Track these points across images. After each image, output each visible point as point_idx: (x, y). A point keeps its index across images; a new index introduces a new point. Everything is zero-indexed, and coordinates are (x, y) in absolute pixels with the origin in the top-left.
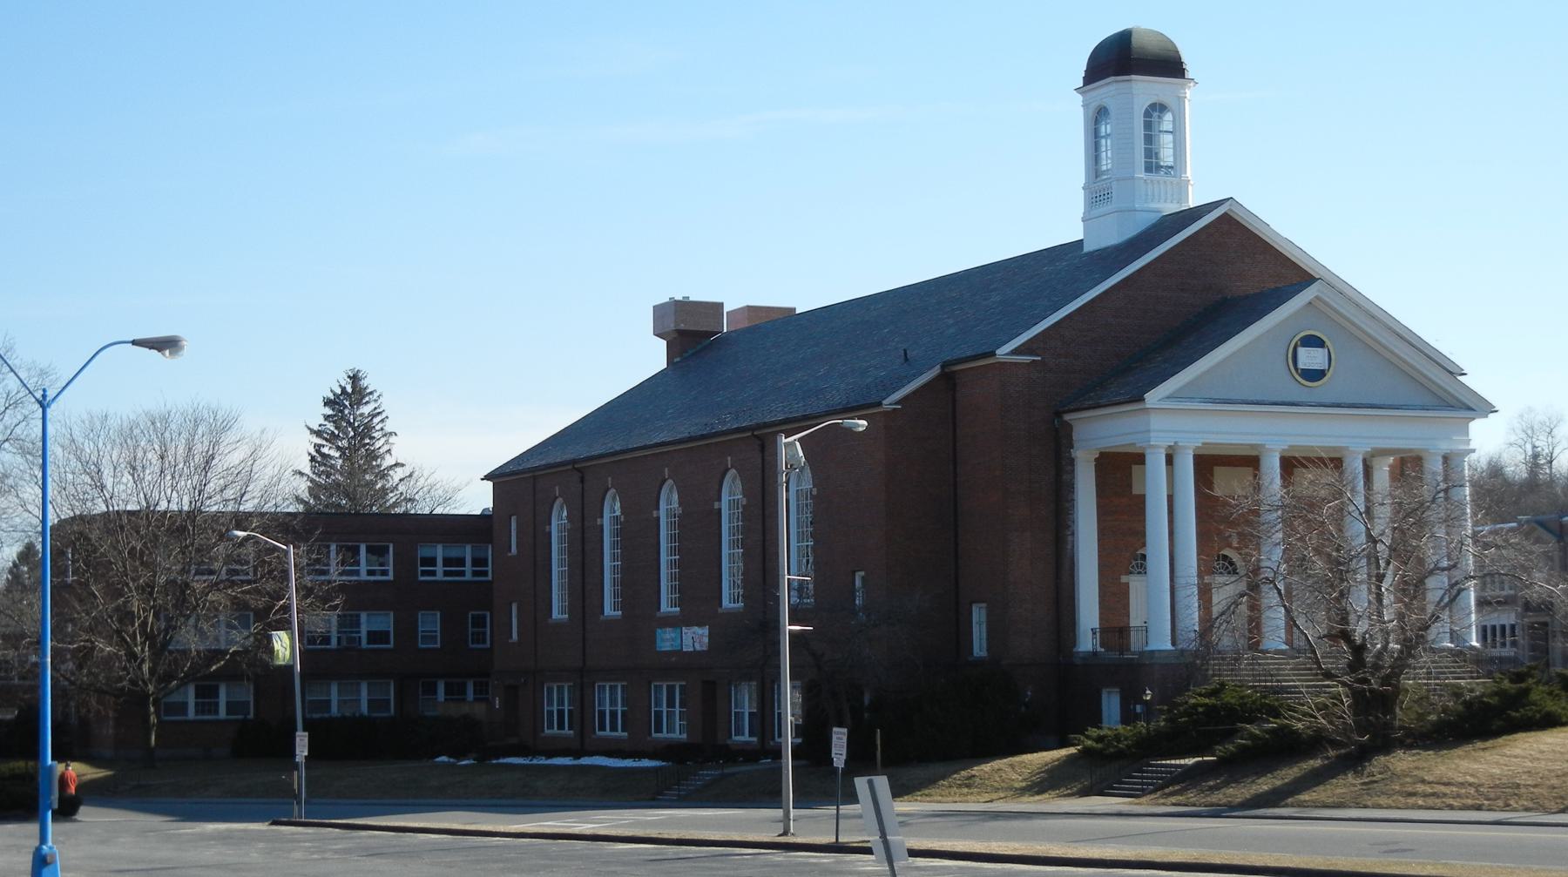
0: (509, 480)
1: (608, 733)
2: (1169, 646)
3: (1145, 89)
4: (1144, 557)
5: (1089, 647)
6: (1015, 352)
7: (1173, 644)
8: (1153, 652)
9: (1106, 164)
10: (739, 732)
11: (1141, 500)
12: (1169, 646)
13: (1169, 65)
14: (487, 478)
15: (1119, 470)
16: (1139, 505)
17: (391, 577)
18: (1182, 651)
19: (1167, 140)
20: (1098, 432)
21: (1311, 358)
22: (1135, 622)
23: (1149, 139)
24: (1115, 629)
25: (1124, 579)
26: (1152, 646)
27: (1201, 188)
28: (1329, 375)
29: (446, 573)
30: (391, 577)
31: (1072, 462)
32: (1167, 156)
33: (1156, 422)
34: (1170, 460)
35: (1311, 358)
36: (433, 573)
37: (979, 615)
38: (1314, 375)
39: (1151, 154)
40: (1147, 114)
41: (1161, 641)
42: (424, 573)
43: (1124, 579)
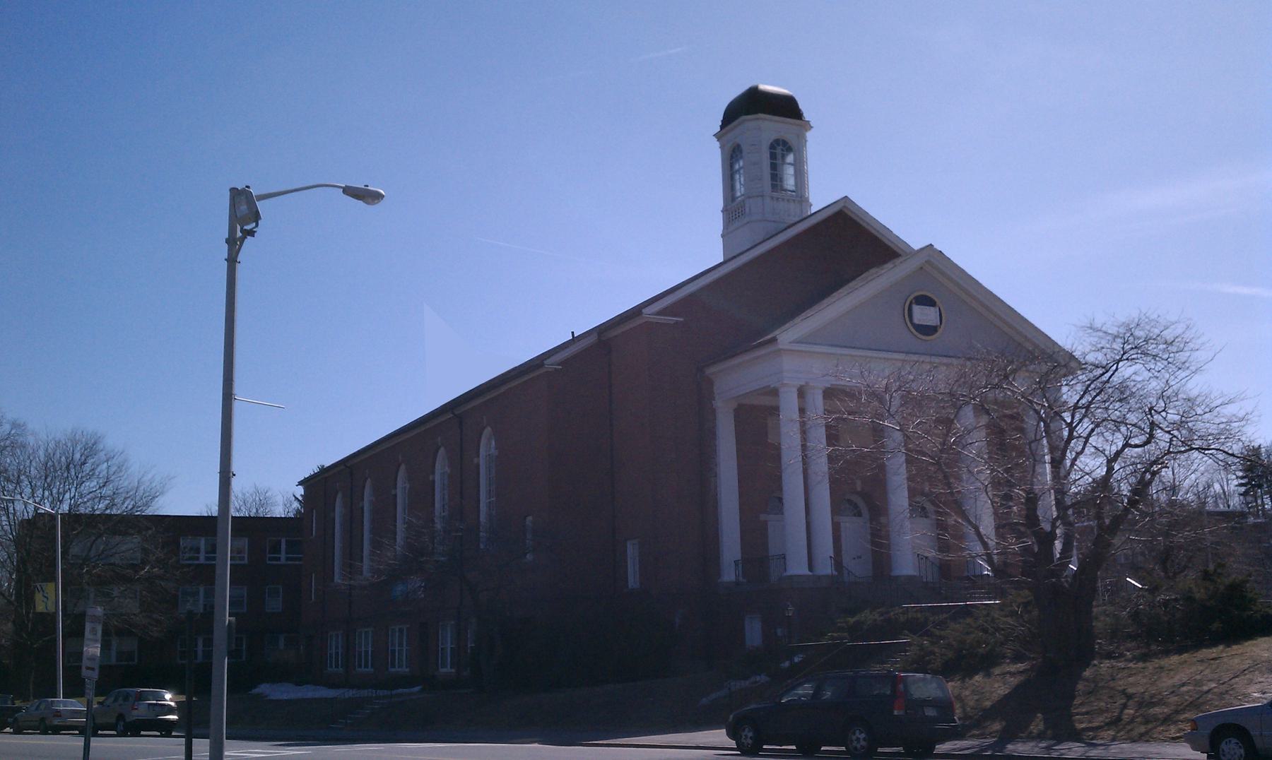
0: (319, 486)
1: (363, 669)
2: (806, 571)
3: (769, 127)
4: (780, 500)
5: (733, 578)
6: (659, 313)
7: (811, 567)
8: (791, 577)
9: (740, 190)
10: (444, 666)
11: (778, 448)
12: (806, 571)
13: (786, 107)
14: (300, 483)
15: (757, 420)
16: (775, 454)
17: (246, 561)
18: (819, 577)
19: (789, 172)
20: (736, 380)
21: (924, 315)
22: (773, 550)
23: (774, 167)
24: (758, 553)
25: (763, 517)
26: (790, 572)
27: (820, 197)
28: (940, 331)
29: (287, 559)
30: (246, 561)
31: (714, 411)
32: (790, 182)
33: (788, 363)
34: (801, 393)
35: (924, 315)
36: (279, 559)
37: (632, 550)
38: (928, 330)
39: (776, 178)
40: (772, 147)
41: (798, 567)
42: (270, 559)
43: (763, 517)
